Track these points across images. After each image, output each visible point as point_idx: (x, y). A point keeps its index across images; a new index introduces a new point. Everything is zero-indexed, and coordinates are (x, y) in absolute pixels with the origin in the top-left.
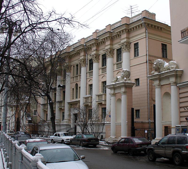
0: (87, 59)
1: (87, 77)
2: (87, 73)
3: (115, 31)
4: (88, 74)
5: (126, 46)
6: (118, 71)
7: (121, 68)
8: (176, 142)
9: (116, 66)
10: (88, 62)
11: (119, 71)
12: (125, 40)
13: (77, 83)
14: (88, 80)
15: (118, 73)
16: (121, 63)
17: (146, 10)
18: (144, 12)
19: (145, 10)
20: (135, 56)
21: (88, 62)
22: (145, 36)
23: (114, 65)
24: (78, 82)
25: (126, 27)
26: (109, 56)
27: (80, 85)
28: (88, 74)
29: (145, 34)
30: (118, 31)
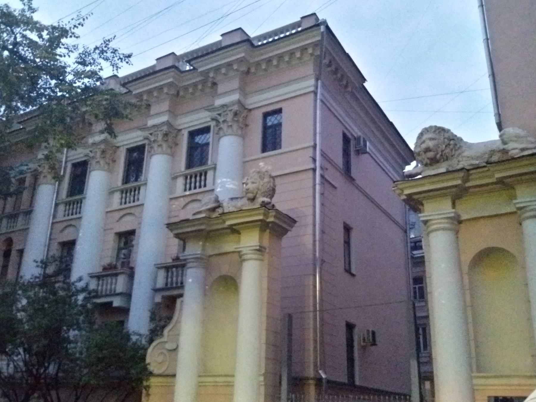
0: (66, 162)
1: (54, 217)
2: (57, 205)
3: (202, 66)
4: (61, 208)
5: (236, 114)
6: (122, 213)
7: (78, 216)
8: (424, 369)
9: (180, 182)
10: (65, 172)
11: (69, 223)
12: (164, 118)
13: (12, 235)
14: (60, 227)
15: (124, 219)
16: (80, 202)
17: (175, 52)
18: (171, 57)
19: (240, 29)
20: (264, 149)
21: (65, 172)
22: (312, 89)
23: (175, 178)
24: (136, 209)
25: (174, 77)
26: (160, 149)
27: (25, 240)
28: (61, 208)
29: (312, 82)
30: (162, 83)
